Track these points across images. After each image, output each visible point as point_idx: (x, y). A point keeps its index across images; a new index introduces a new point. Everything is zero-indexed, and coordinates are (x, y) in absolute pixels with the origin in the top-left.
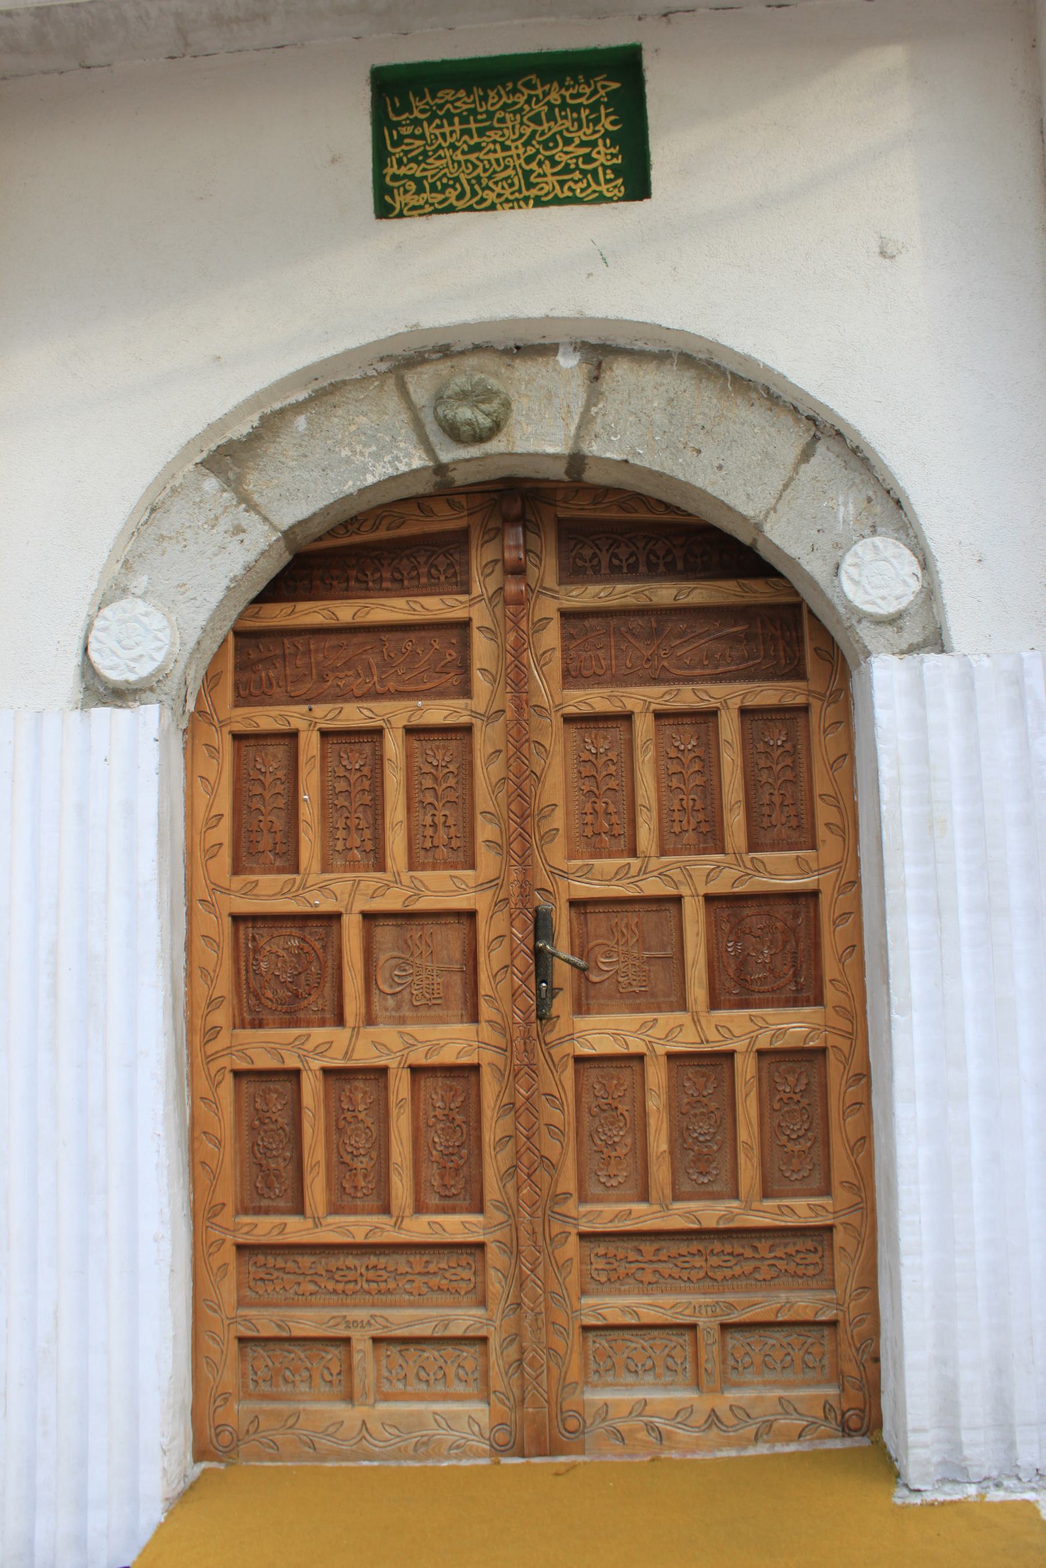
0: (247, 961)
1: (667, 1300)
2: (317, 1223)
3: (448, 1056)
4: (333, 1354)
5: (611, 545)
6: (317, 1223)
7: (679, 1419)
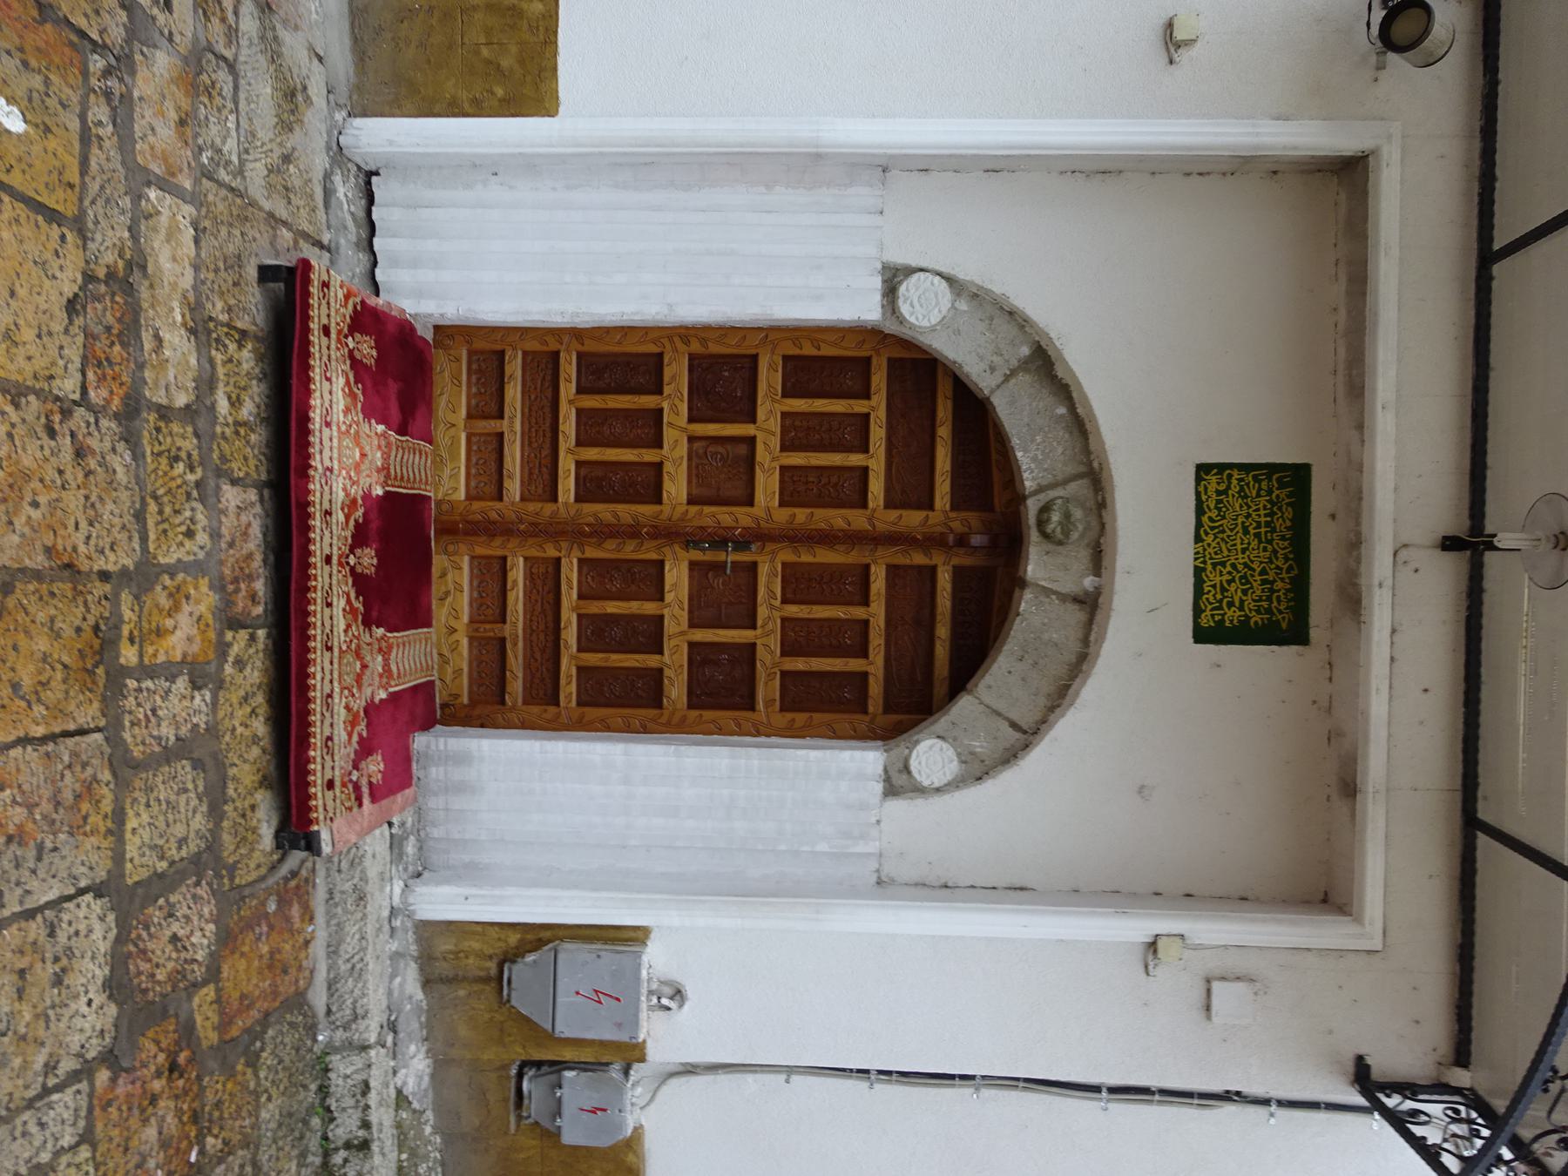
2: (571, 402)
3: (668, 485)
4: (494, 407)
6: (571, 402)
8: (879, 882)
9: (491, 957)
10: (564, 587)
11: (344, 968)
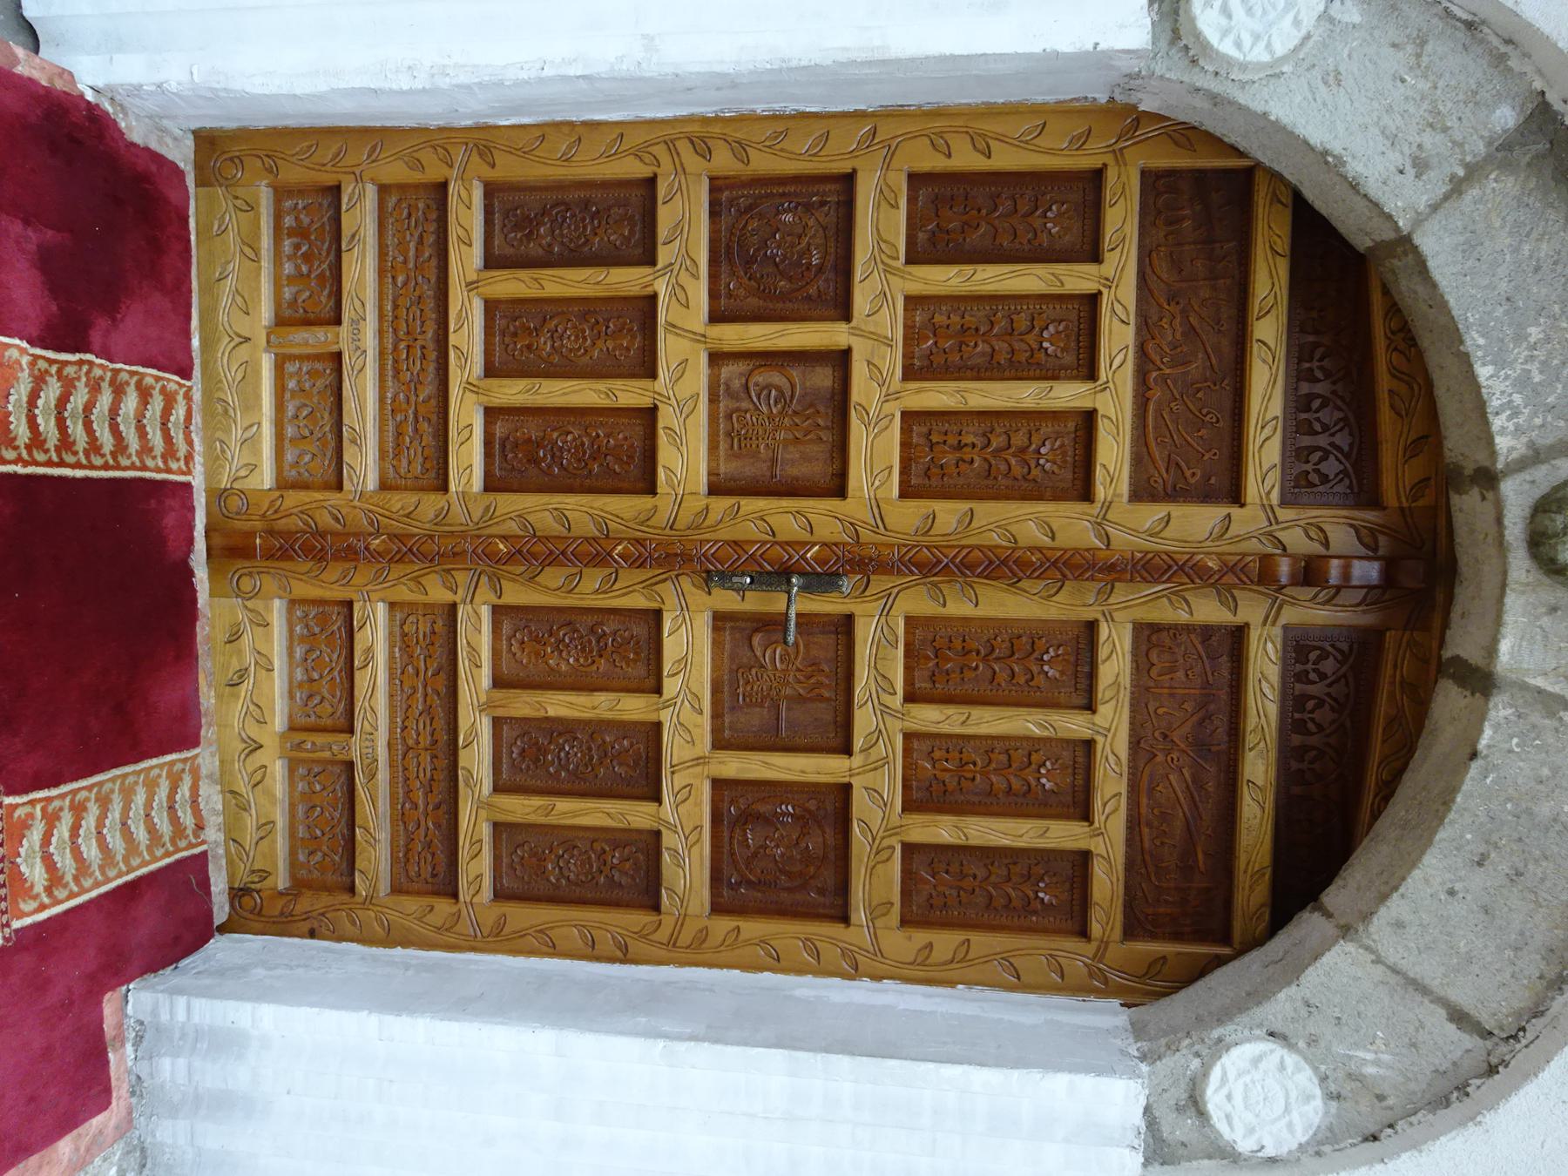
0: (796, 194)
2: (471, 286)
3: (667, 455)
5: (1335, 700)
6: (471, 286)
7: (252, 707)
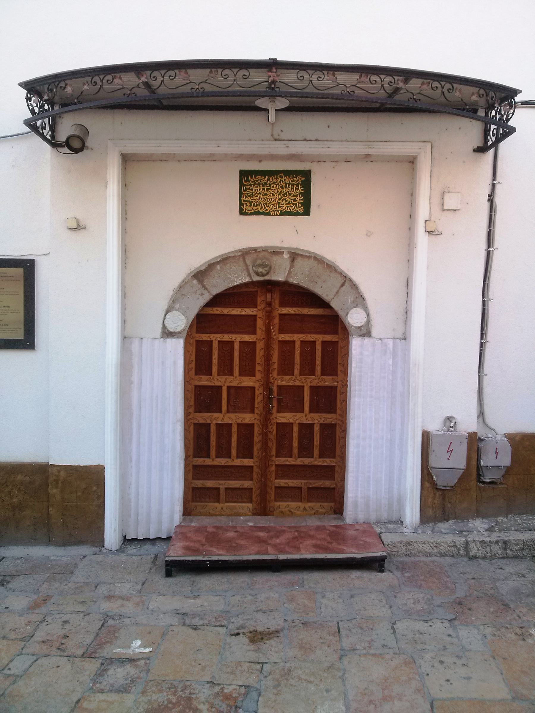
1: (295, 481)
6: (213, 460)
8: (405, 339)
9: (435, 494)
10: (287, 463)
11: (436, 550)
